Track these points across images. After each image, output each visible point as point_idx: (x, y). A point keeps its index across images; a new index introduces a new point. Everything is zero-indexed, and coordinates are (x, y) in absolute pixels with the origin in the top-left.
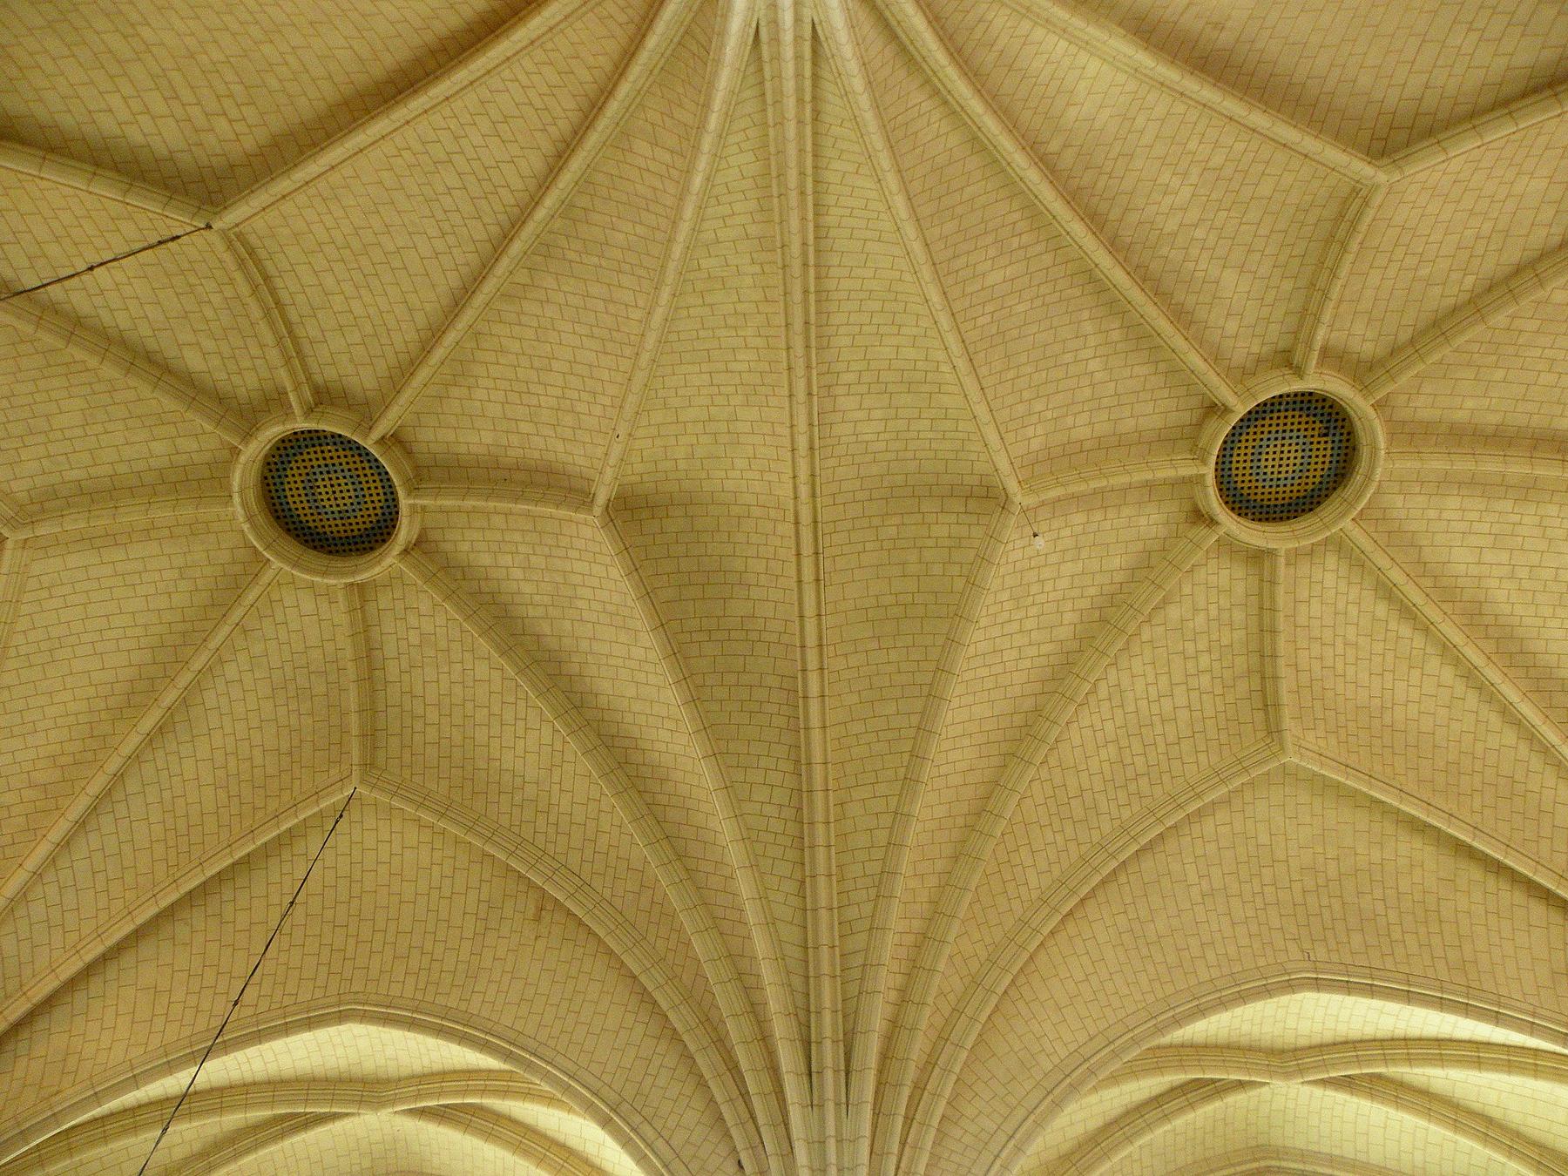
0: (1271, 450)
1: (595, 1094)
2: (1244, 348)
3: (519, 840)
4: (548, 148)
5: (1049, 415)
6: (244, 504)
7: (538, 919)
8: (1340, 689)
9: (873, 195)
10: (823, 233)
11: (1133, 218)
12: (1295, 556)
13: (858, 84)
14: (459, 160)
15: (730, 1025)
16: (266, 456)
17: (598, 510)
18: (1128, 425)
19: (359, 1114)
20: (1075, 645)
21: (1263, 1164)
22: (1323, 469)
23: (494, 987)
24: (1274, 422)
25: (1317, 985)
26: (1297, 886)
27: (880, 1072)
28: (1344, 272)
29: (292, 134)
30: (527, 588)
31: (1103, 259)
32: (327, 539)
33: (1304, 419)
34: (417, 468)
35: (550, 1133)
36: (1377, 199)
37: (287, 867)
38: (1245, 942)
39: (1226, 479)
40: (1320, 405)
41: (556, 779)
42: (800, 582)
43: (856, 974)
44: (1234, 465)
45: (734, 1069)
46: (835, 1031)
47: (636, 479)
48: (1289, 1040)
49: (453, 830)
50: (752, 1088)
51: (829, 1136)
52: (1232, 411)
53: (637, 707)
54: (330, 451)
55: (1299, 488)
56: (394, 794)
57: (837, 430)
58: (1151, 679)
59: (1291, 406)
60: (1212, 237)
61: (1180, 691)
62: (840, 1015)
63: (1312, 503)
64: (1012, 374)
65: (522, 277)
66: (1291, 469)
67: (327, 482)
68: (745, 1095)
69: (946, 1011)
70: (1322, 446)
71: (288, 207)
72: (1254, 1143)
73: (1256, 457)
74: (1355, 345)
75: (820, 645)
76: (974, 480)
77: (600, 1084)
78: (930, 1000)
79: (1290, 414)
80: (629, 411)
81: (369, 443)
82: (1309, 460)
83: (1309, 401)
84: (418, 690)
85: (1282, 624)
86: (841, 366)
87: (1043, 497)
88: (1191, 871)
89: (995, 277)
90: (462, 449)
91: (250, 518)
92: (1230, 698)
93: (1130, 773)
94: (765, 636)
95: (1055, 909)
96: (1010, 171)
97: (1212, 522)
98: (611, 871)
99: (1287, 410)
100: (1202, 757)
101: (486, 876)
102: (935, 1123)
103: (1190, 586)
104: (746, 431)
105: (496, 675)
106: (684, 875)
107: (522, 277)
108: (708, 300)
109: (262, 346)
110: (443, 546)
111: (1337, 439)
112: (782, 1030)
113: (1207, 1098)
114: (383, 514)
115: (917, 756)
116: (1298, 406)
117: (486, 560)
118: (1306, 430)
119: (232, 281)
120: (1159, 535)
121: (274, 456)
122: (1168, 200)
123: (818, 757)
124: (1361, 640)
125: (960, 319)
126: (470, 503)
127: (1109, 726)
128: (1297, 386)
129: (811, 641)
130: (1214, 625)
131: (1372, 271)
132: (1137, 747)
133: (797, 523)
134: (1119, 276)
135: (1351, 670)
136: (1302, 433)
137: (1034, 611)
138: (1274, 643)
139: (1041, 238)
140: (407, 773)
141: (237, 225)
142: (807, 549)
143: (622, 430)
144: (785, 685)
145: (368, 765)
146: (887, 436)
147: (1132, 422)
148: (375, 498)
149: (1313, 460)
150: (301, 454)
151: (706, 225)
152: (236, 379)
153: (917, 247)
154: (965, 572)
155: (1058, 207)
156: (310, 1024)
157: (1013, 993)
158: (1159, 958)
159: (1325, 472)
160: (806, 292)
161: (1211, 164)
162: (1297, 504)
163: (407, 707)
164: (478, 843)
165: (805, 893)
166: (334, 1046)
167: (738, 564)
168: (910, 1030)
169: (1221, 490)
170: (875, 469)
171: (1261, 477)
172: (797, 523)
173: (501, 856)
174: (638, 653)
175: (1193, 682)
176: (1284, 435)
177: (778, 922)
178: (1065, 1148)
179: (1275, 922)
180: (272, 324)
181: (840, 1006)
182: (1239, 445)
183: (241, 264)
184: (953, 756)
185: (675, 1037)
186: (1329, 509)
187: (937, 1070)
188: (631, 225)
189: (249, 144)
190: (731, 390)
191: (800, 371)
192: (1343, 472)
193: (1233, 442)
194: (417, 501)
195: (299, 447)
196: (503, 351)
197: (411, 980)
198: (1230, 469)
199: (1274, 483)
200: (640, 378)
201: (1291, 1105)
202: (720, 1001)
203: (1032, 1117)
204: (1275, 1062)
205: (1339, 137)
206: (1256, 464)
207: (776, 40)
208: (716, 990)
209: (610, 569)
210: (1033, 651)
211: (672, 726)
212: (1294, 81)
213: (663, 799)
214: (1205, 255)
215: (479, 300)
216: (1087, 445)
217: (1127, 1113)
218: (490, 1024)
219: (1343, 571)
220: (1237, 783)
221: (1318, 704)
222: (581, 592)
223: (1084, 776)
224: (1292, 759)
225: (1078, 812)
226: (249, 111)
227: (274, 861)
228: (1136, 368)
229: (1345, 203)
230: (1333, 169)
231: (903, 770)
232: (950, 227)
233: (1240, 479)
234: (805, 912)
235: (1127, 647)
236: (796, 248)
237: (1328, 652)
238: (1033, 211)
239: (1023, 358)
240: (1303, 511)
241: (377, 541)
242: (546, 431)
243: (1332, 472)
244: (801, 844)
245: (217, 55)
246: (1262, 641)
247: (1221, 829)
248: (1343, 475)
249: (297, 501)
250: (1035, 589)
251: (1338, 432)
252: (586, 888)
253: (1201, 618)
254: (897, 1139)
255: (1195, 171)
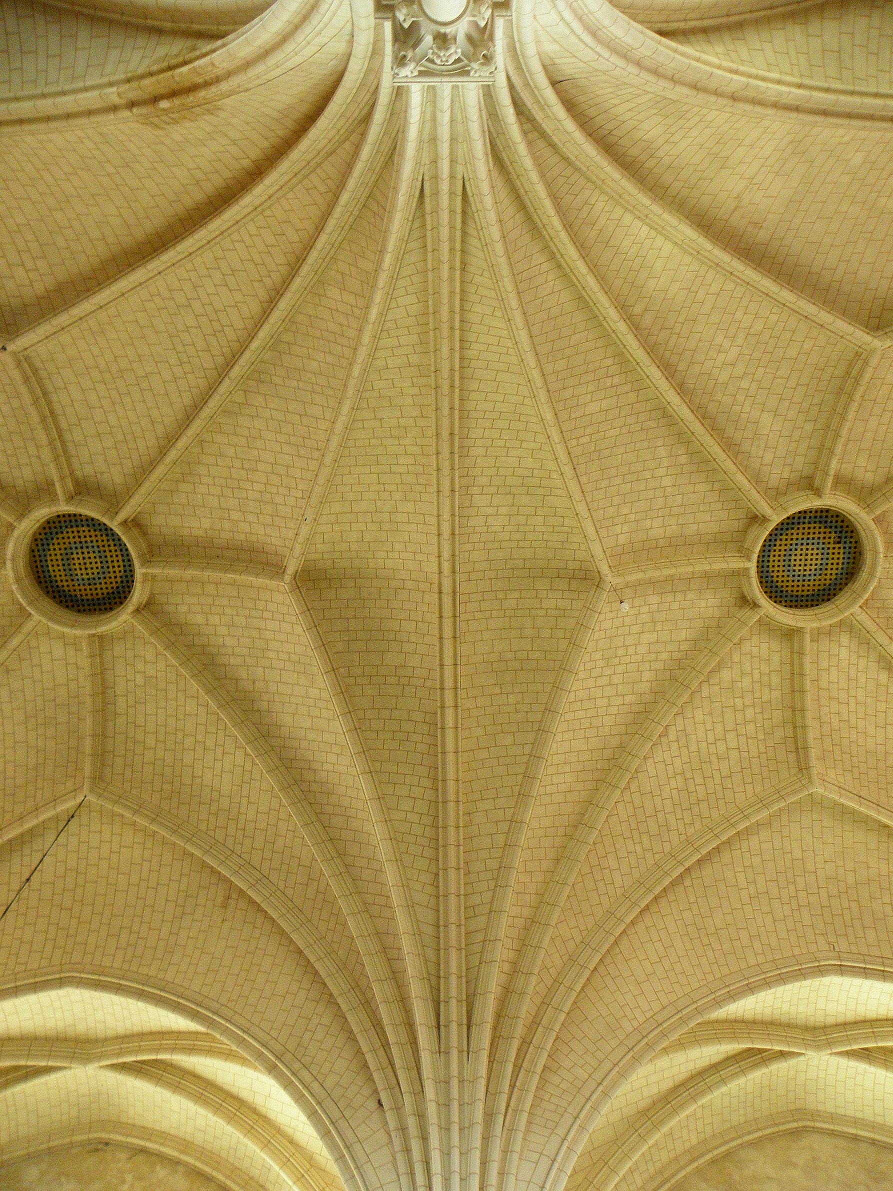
0: (798, 552)
1: (263, 1045)
2: (778, 475)
3: (213, 841)
4: (262, 294)
5: (632, 517)
6: (15, 570)
7: (225, 906)
8: (854, 739)
9: (504, 333)
10: (466, 363)
11: (696, 369)
12: (817, 635)
13: (495, 233)
14: (196, 305)
15: (375, 987)
16: (35, 533)
17: (287, 578)
18: (691, 529)
19: (71, 1068)
20: (651, 697)
21: (801, 1124)
22: (837, 569)
23: (187, 960)
24: (801, 531)
25: (841, 970)
26: (823, 893)
27: (495, 1028)
28: (851, 416)
29: (72, 282)
30: (230, 642)
31: (674, 398)
32: (77, 601)
33: (822, 530)
34: (150, 546)
35: (226, 1087)
36: (874, 362)
37: (26, 860)
38: (783, 935)
39: (765, 574)
40: (834, 520)
41: (245, 793)
42: (441, 638)
43: (477, 948)
44: (771, 564)
45: (377, 1025)
46: (459, 992)
47: (318, 556)
48: (820, 1019)
49: (162, 832)
50: (391, 1038)
51: (454, 1146)
52: (769, 520)
53: (311, 736)
54: (84, 531)
55: (820, 582)
56: (116, 802)
57: (473, 522)
58: (709, 726)
59: (813, 520)
60: (754, 386)
61: (731, 736)
62: (464, 980)
63: (829, 594)
64: (604, 484)
65: (239, 397)
66: (813, 567)
67: (81, 556)
68: (386, 1046)
69: (549, 982)
70: (836, 551)
71: (65, 338)
72: (792, 1107)
73: (787, 558)
74: (859, 474)
75: (456, 688)
76: (576, 565)
77: (269, 1038)
78: (536, 971)
79: (812, 525)
80: (314, 500)
81: (114, 525)
82: (828, 551)
83: (826, 517)
84: (140, 720)
85: (808, 685)
86: (477, 471)
87: (628, 579)
88: (741, 877)
89: (593, 407)
90: (186, 532)
91: (18, 580)
92: (770, 743)
93: (693, 798)
94: (414, 681)
95: (635, 904)
96: (606, 325)
97: (755, 605)
98: (285, 867)
99: (810, 523)
100: (749, 788)
101: (186, 871)
102: (539, 1069)
103: (739, 655)
104: (404, 521)
105: (202, 711)
106: (343, 870)
107: (239, 397)
108: (379, 414)
109: (38, 447)
110: (166, 608)
111: (847, 545)
112: (416, 990)
113: (756, 1066)
114: (122, 582)
115: (528, 777)
116: (818, 520)
117: (199, 619)
118: (824, 538)
119: (18, 395)
120: (715, 615)
121: (40, 534)
122: (722, 356)
123: (451, 774)
124: (869, 700)
125: (567, 436)
126: (190, 573)
127: (677, 762)
128: (816, 503)
129: (449, 683)
130: (757, 686)
131: (871, 418)
132: (699, 780)
133: (440, 593)
134: (685, 412)
135: (861, 723)
136: (821, 541)
137: (619, 669)
138: (803, 700)
139: (628, 380)
140: (127, 786)
141: (25, 349)
142: (447, 612)
143: (309, 515)
144: (427, 720)
145: (98, 779)
146: (510, 528)
147: (694, 527)
148: (117, 569)
149: (830, 562)
150: (62, 533)
151: (379, 354)
152: (16, 473)
153: (536, 374)
154: (568, 636)
155: (640, 355)
156: (36, 987)
157: (601, 969)
158: (716, 946)
159: (839, 571)
160: (452, 409)
161: (752, 331)
162: (818, 595)
163: (131, 734)
164: (180, 842)
165: (438, 882)
166: (54, 1009)
167: (395, 625)
168: (520, 994)
169: (761, 582)
170: (500, 554)
171: (791, 573)
172: (440, 593)
173: (198, 853)
174: (314, 692)
175: (741, 729)
176: (808, 541)
177: (417, 907)
178: (642, 1105)
179: (807, 920)
180: (46, 428)
181: (464, 974)
182: (775, 548)
183: (26, 380)
184: (557, 779)
185: (331, 1000)
186: (841, 600)
187: (540, 1029)
188: (322, 355)
189: (40, 289)
190: (393, 487)
191: (446, 471)
192: (852, 571)
193: (770, 546)
194: (149, 571)
195: (61, 527)
196: (221, 455)
197: (120, 954)
198: (768, 566)
199: (801, 578)
200: (325, 473)
201: (822, 1075)
202: (368, 969)
203: (617, 1069)
204: (808, 1036)
205: (845, 313)
206: (787, 563)
207: (436, 193)
208: (366, 960)
209: (295, 627)
210: (619, 701)
211: (336, 749)
212: (813, 270)
213: (329, 809)
214: (749, 401)
215: (205, 413)
216: (661, 543)
217: (692, 1078)
218: (182, 990)
219: (854, 646)
220: (776, 807)
221: (836, 749)
222: (272, 645)
223: (658, 800)
224: (818, 789)
225: (654, 829)
226: (40, 263)
227: (16, 856)
228: (698, 486)
229: (851, 364)
230: (842, 337)
231: (518, 787)
232: (561, 365)
233: (775, 574)
234: (438, 897)
235: (690, 702)
236: (445, 373)
237: (844, 709)
238: (623, 360)
239: (613, 472)
240: (823, 600)
241: (116, 603)
242: (251, 518)
243: (844, 571)
244: (437, 844)
245: (20, 219)
246: (793, 699)
247: (764, 846)
248: (852, 574)
249: (56, 570)
250: (621, 652)
251: (848, 540)
252: (265, 881)
253: (747, 680)
254: (507, 1083)
255: (741, 335)
